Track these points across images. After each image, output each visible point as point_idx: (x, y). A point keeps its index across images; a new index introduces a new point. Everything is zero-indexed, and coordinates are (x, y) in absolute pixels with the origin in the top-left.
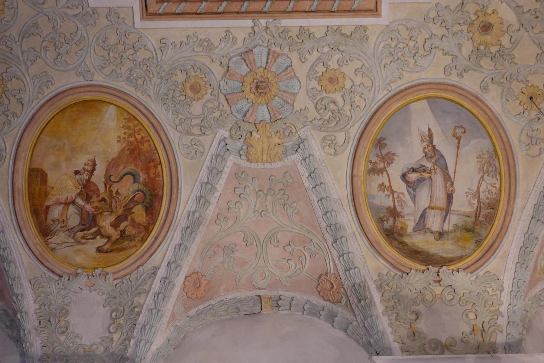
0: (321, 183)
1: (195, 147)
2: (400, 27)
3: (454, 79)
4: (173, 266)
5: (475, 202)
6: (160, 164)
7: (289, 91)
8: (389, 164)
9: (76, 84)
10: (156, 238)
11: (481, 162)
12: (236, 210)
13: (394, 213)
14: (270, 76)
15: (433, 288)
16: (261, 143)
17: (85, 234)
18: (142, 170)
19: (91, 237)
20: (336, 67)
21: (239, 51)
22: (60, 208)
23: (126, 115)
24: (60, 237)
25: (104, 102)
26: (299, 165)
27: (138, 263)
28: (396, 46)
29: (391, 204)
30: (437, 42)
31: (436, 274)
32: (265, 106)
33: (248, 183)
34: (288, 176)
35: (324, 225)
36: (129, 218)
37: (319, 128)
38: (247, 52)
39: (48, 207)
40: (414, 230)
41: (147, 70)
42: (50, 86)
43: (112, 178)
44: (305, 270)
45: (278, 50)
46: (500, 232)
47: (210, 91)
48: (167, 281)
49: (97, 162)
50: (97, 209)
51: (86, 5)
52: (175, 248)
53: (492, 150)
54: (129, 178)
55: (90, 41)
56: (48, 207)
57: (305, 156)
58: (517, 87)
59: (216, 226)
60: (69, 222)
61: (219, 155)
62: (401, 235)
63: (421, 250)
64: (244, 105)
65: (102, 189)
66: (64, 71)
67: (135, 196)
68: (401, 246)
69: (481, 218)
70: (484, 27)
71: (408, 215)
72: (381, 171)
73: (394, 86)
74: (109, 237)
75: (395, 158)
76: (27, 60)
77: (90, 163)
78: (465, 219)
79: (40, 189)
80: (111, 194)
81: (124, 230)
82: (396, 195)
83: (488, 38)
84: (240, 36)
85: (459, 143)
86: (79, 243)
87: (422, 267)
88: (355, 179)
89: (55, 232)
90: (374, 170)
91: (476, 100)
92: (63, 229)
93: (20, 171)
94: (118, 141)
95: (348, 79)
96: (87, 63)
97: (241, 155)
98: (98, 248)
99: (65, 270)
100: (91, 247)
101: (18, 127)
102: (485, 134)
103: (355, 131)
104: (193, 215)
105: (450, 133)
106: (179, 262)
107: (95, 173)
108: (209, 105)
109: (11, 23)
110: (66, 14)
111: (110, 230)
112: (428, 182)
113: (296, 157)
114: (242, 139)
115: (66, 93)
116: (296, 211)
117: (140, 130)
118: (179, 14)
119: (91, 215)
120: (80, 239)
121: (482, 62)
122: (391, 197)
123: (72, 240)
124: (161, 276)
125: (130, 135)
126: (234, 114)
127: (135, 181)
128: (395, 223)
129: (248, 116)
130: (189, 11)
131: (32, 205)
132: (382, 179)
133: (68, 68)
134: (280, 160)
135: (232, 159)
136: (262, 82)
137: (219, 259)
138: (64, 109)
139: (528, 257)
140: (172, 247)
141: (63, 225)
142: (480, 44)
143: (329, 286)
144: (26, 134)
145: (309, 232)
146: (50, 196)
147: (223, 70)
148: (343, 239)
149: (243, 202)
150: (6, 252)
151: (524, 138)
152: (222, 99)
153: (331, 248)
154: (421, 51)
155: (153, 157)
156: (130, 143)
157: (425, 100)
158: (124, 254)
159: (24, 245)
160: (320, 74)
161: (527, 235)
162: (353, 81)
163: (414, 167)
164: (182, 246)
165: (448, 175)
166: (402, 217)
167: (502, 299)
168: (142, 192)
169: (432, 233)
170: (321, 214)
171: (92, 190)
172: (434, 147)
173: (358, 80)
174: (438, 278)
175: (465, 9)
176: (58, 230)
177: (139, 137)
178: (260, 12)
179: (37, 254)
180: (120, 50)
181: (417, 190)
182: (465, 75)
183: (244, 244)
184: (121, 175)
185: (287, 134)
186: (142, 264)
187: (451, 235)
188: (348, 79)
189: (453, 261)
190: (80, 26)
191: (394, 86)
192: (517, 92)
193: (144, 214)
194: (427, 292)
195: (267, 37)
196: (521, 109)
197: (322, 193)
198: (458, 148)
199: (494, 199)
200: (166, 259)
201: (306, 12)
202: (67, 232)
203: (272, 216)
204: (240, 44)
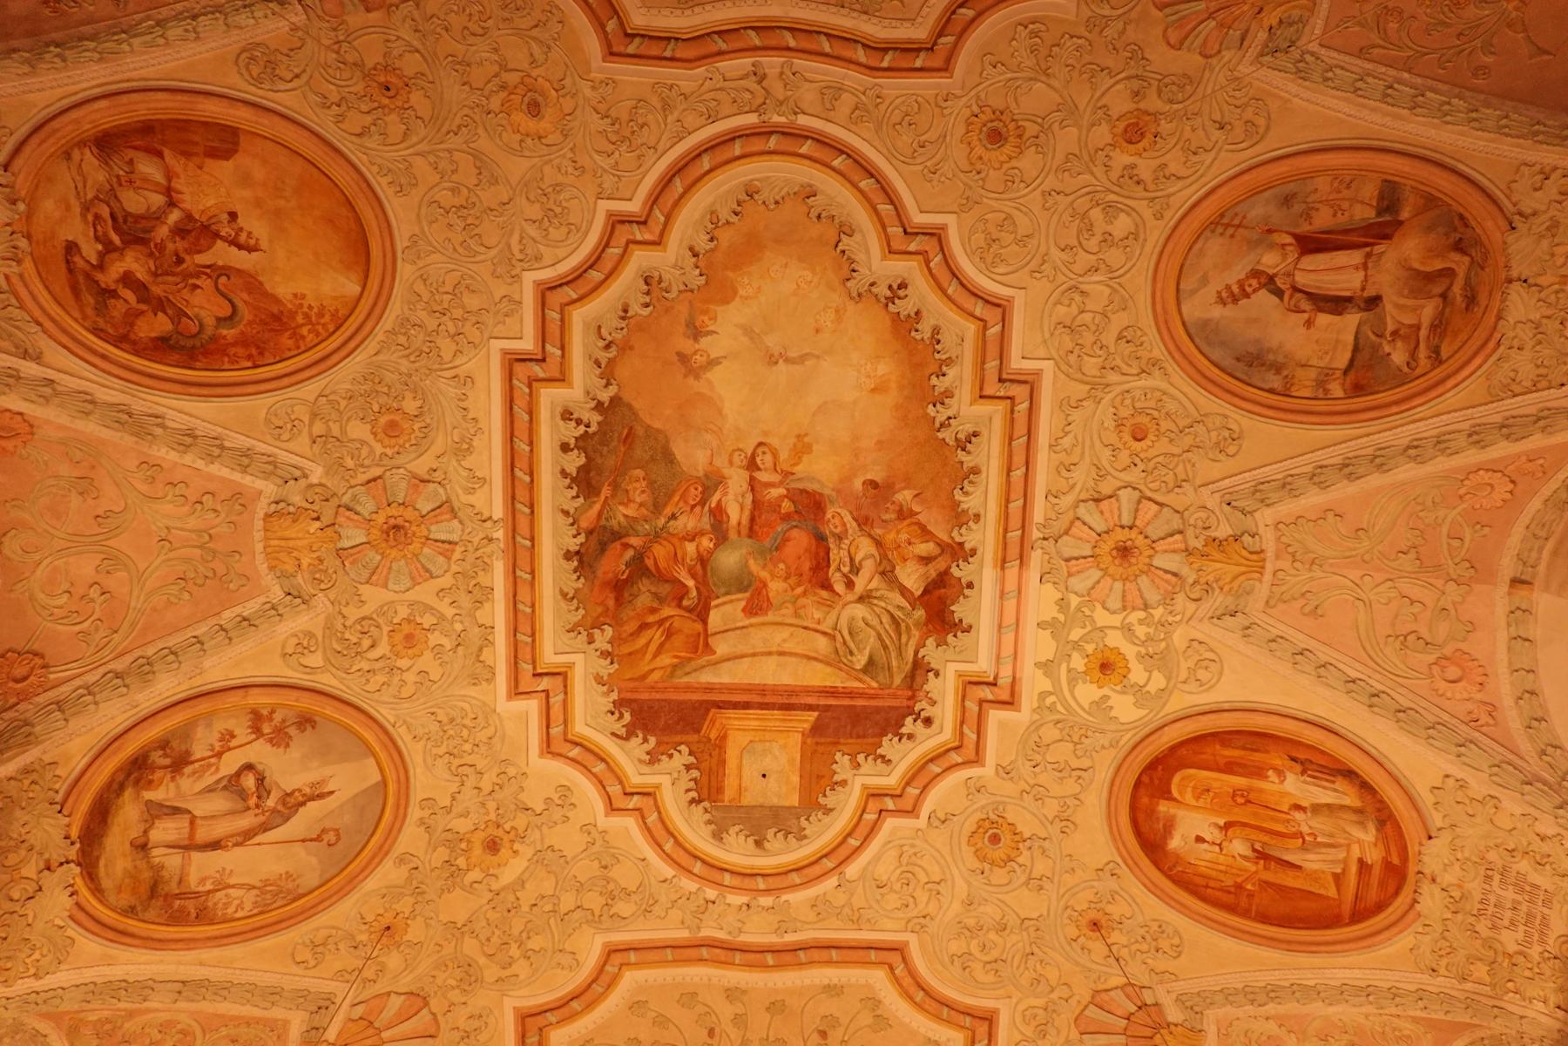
0: (230, 639)
1: (289, 426)
2: (491, 730)
3: (415, 813)
4: (48, 391)
5: (209, 887)
6: (256, 366)
7: (391, 576)
8: (271, 740)
9: (396, 232)
10: (104, 357)
11: (280, 879)
12: (169, 498)
13: (180, 763)
14: (415, 546)
15: (33, 861)
16: (300, 535)
17: (105, 221)
18: (242, 333)
19: (100, 234)
20: (431, 644)
21: (454, 498)
22: (159, 177)
23: (343, 312)
24: (97, 174)
25: (367, 277)
26: (262, 599)
27: (48, 324)
28: (464, 726)
29: (198, 755)
30: (470, 782)
31: (63, 860)
32: (364, 540)
33: (223, 515)
34: (241, 583)
35: (150, 651)
36: (143, 307)
37: (329, 626)
38: (452, 510)
39: (160, 155)
40: (149, 803)
41: (422, 352)
42: (393, 189)
43: (223, 279)
44: (49, 624)
45: (457, 555)
46: (152, 939)
47: (389, 452)
48: (11, 381)
49: (254, 254)
50: (161, 247)
51: (526, 266)
52: (87, 394)
53: (301, 891)
54: (226, 311)
55: (470, 266)
56: (160, 155)
57: (280, 608)
58: (405, 905)
59: (137, 463)
60: (131, 193)
61: (276, 467)
62: (137, 782)
63: (109, 821)
64: (367, 506)
65: (202, 259)
66: (418, 215)
67: (190, 318)
68: (115, 786)
69: (178, 902)
70: (494, 843)
71: (178, 787)
72: (257, 730)
73: (403, 730)
74: (101, 267)
75: (281, 750)
76: (437, 156)
77: (252, 242)
78: (176, 879)
79: (196, 144)
80: (191, 276)
81: (120, 297)
82: (213, 760)
83: (478, 850)
84: (478, 499)
85: (311, 840)
86: (86, 208)
87: (74, 833)
88: (241, 692)
89: (107, 164)
90: (257, 720)
91: (382, 852)
92: (115, 180)
93: (231, 111)
94: (295, 295)
95: (411, 662)
96: (433, 256)
97: (277, 503)
98: (76, 245)
99: (21, 177)
100: (76, 230)
101: (316, 119)
102: (328, 876)
103: (327, 681)
104: (157, 425)
105: (328, 824)
106: (57, 400)
107: (234, 249)
108: (365, 452)
109: (498, 141)
110: (512, 232)
111: (117, 268)
112: (240, 805)
113: (277, 593)
114: (308, 506)
115: (381, 216)
116: (173, 599)
117: (318, 335)
118: (511, 409)
119: (147, 236)
120: (93, 210)
121: (441, 849)
122: (210, 753)
123: (90, 196)
124: (22, 369)
125: (307, 316)
126: (350, 491)
127: (219, 320)
128: (160, 768)
129: (348, 513)
130: (516, 425)
131: (165, 125)
132: (243, 733)
133: (425, 223)
134: (271, 568)
135: (269, 488)
136: (406, 534)
137: (65, 469)
138: (353, 208)
139: (107, 997)
140: (85, 386)
141: (123, 180)
142: (469, 841)
143: (19, 672)
144: (307, 134)
145: (133, 625)
146: (183, 160)
147: (422, 473)
148: (124, 690)
149: (186, 509)
150: (56, 60)
151: (324, 933)
152: (376, 472)
153: (101, 670)
154: (456, 762)
155: (267, 354)
156: (293, 315)
157: (379, 778)
158: (67, 295)
159: (74, 99)
160: (419, 620)
161: (150, 982)
162: (408, 669)
163: (267, 782)
164: (90, 407)
165: (255, 835)
166: (173, 779)
167: (20, 981)
168: (199, 333)
169: (145, 832)
170: (170, 644)
171: (198, 239)
172: (303, 804)
173: (411, 677)
174: (54, 864)
175: (519, 814)
176: (111, 168)
177: (304, 331)
178: (514, 530)
179: (55, 124)
180: (453, 311)
181: (226, 793)
182: (423, 828)
183: (100, 511)
184: (232, 296)
185: (317, 576)
186: (45, 331)
187: (142, 864)
188: (411, 662)
189: (92, 879)
190: (493, 252)
191: (403, 730)
192: (398, 907)
193: (153, 335)
194: (23, 853)
195: (476, 540)
196: (370, 918)
197: (213, 642)
198: (303, 841)
199: (215, 914)
200: (61, 375)
201: (515, 596)
202: (108, 187)
203: (162, 557)
204: (465, 499)
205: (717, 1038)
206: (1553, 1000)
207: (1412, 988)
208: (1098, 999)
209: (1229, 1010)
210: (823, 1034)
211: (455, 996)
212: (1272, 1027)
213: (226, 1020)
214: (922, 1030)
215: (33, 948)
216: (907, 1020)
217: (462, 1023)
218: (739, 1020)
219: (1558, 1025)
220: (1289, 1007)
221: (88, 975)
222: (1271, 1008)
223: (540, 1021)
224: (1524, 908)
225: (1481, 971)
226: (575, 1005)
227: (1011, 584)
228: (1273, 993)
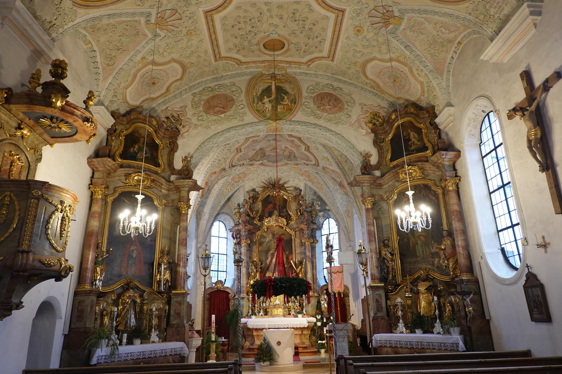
205: (263, 15)
206: (494, 29)
207: (463, 17)
208: (376, 8)
209: (412, 15)
210: (294, 14)
211: (185, 9)
212: (423, 20)
213: (124, 22)
214: (323, 13)
215: (68, 15)
216: (319, 10)
217: (188, 15)
218: (269, 10)
219: (492, 35)
220: (429, 16)
221: (84, 18)
222: (424, 15)
223: (211, 13)
224: (500, 4)
225: (481, 17)
226: (220, 9)
227: (357, 305)
228: (426, 12)
